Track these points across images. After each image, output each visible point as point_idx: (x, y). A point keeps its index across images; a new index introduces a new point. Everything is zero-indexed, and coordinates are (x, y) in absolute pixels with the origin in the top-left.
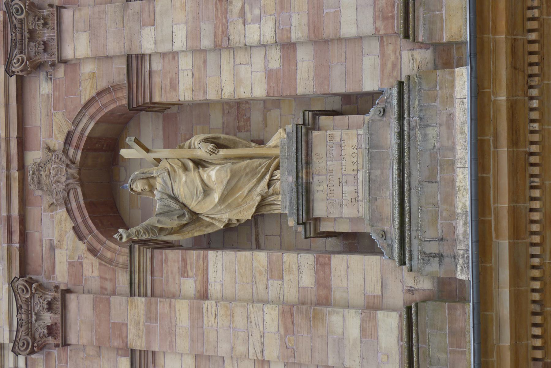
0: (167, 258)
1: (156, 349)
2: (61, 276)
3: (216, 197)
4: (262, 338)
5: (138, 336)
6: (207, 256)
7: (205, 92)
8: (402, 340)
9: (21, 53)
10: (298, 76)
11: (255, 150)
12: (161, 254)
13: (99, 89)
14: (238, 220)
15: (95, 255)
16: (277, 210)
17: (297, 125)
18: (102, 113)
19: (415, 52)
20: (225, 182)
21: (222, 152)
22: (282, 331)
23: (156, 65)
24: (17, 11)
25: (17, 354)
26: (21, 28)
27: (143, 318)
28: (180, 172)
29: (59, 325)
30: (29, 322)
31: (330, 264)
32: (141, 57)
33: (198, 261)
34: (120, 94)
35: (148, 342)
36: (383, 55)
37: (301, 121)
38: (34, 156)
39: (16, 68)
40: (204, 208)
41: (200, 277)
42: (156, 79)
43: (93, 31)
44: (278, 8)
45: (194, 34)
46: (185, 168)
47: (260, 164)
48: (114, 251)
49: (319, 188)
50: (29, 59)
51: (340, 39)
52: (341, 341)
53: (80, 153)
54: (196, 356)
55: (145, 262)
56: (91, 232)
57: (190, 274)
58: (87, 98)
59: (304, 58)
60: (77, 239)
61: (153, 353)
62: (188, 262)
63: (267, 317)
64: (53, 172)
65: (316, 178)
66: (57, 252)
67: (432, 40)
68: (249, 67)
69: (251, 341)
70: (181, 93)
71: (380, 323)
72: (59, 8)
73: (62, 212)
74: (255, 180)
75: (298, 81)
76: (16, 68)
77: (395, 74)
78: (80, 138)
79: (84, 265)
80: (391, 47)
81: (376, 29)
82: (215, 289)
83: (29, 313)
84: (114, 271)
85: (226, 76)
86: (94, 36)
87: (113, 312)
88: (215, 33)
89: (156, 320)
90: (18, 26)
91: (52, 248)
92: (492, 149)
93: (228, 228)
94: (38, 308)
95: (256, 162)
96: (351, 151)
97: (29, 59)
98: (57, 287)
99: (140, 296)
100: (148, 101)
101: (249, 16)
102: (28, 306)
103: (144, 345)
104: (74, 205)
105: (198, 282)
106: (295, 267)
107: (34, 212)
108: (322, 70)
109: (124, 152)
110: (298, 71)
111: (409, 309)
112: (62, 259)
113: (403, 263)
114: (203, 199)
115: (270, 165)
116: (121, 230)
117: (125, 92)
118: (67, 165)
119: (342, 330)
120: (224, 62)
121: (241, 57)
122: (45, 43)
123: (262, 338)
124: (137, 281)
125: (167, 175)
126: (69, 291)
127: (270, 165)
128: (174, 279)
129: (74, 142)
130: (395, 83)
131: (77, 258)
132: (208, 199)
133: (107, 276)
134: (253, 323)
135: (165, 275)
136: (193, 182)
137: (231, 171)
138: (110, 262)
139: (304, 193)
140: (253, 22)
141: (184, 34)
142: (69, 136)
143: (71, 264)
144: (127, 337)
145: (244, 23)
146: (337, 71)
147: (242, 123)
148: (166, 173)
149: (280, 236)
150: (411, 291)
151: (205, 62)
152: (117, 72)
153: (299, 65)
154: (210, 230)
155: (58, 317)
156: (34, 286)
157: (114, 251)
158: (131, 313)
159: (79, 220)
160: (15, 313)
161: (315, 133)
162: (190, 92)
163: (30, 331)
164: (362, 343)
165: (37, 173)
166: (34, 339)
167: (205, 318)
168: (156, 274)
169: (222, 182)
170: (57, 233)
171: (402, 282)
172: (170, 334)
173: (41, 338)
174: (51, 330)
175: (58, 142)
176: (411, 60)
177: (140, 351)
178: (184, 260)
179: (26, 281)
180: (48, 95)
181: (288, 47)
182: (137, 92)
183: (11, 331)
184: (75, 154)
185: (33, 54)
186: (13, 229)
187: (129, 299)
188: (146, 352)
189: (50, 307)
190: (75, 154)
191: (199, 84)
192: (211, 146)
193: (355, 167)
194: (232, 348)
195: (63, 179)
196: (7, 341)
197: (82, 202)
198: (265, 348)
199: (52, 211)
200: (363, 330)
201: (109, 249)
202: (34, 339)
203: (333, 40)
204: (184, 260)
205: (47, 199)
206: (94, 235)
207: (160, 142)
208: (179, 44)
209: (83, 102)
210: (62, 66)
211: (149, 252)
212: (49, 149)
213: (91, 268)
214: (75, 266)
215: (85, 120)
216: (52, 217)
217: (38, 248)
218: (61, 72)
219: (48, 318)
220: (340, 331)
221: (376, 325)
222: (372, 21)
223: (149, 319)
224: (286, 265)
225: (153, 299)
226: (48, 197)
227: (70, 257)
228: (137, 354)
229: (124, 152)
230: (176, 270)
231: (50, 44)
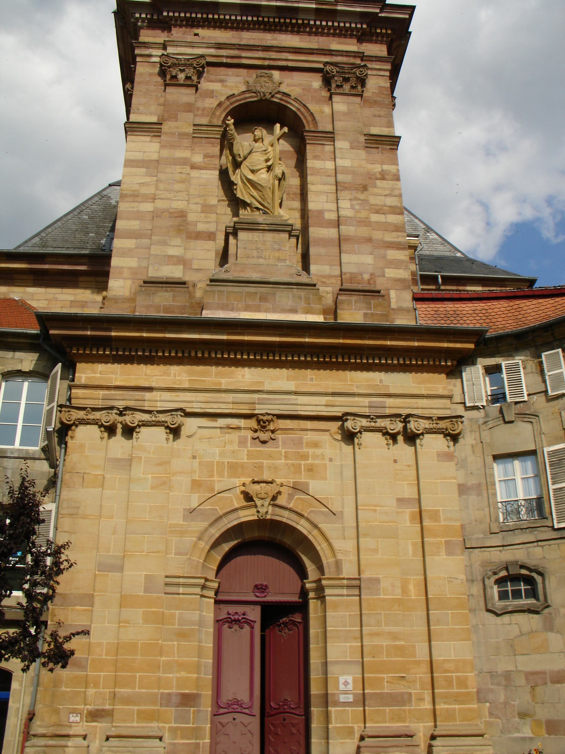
0: (216, 146)
2: (204, 85)
3: (251, 176)
4: (168, 199)
5: (170, 128)
6: (216, 170)
7: (312, 175)
8: (166, 278)
9: (337, 72)
11: (277, 202)
12: (217, 144)
13: (315, 115)
14: (236, 189)
15: (218, 105)
16: (242, 212)
17: (292, 226)
19: (331, 294)
20: (259, 182)
22: (172, 210)
23: (328, 148)
24: (361, 72)
25: (160, 57)
26: (351, 73)
28: (266, 157)
29: (177, 82)
30: (179, 65)
31: (210, 240)
32: (333, 140)
33: (213, 164)
34: (311, 126)
35: (166, 133)
36: (330, 276)
38: (276, 74)
39: (328, 68)
40: (244, 169)
41: (203, 165)
42: (319, 147)
44: (358, 219)
45: (346, 170)
46: (267, 160)
47: (269, 203)
48: (220, 116)
49: (255, 236)
50: (334, 76)
51: (340, 253)
52: (165, 243)
53: (278, 101)
54: (158, 161)
56: (231, 104)
57: (206, 160)
59: (332, 233)
60: (227, 96)
61: (160, 136)
63: (180, 202)
64: (267, 84)
66: (220, 84)
68: (325, 200)
69: (166, 192)
71: (176, 267)
72: (361, 96)
73: (244, 89)
74: (260, 199)
75: (317, 228)
76: (328, 68)
77: (319, 283)
78: (287, 102)
79: (212, 99)
80: (334, 281)
81: (345, 273)
82: (195, 173)
83: (185, 65)
84: (207, 116)
85: (321, 188)
86: (345, 114)
87: (185, 114)
88: (345, 183)
89: (180, 139)
90: (353, 71)
91: (222, 81)
92: (278, 332)
93: (232, 184)
95: (270, 201)
96: (277, 256)
97: (334, 76)
98: (199, 83)
99: (194, 130)
101: (354, 202)
102: (189, 65)
106: (209, 220)
109: (278, 126)
110: (322, 229)
111: (184, 283)
112: (216, 86)
113: (211, 281)
116: (232, 121)
117: (313, 129)
118: (271, 93)
119: (172, 244)
120: (329, 187)
121: (332, 197)
122: (342, 86)
123: (168, 199)
125: (263, 149)
126: (197, 90)
131: (216, 95)
132: (250, 172)
133: (205, 112)
134: (176, 194)
136: (260, 164)
137: (266, 186)
138: (213, 114)
139: (252, 227)
142: (288, 95)
143: (212, 91)
144: (169, 121)
145: (350, 200)
146: (322, 251)
147: (291, 196)
148: (264, 149)
149: (225, 214)
150: (194, 286)
151: (329, 176)
152: (325, 126)
153: (326, 229)
155: (182, 82)
156: (201, 69)
158: (184, 124)
159: (238, 98)
161: (287, 236)
162: (312, 166)
163: (174, 65)
164: (165, 256)
165: (267, 75)
166: (169, 67)
169: (259, 180)
170: (229, 86)
171: (200, 281)
172: (173, 146)
173: (170, 71)
175: (283, 88)
176: (328, 292)
177: (161, 129)
178: (213, 156)
179: (203, 64)
180: (311, 85)
181: (338, 223)
182: (313, 136)
183: (174, 54)
185: (336, 78)
186: (234, 59)
187: (192, 124)
188: (160, 132)
189: (188, 78)
191: (317, 172)
192: (280, 176)
193: (267, 257)
194: (162, 181)
195: (263, 91)
196: (168, 51)
199: (244, 83)
200: (171, 256)
201: (221, 114)
202: (169, 67)
204: (213, 156)
206: (229, 106)
207: (281, 149)
208: (339, 162)
209: (307, 105)
210: (328, 95)
211: (219, 137)
212: (280, 83)
213: (211, 103)
214: (211, 94)
215: (297, 105)
216: (240, 83)
218: (326, 94)
222: (350, 271)
224: (210, 215)
225: (191, 137)
226: (252, 81)
228: (160, 127)
229: (278, 126)
230: (208, 151)
231: (342, 89)
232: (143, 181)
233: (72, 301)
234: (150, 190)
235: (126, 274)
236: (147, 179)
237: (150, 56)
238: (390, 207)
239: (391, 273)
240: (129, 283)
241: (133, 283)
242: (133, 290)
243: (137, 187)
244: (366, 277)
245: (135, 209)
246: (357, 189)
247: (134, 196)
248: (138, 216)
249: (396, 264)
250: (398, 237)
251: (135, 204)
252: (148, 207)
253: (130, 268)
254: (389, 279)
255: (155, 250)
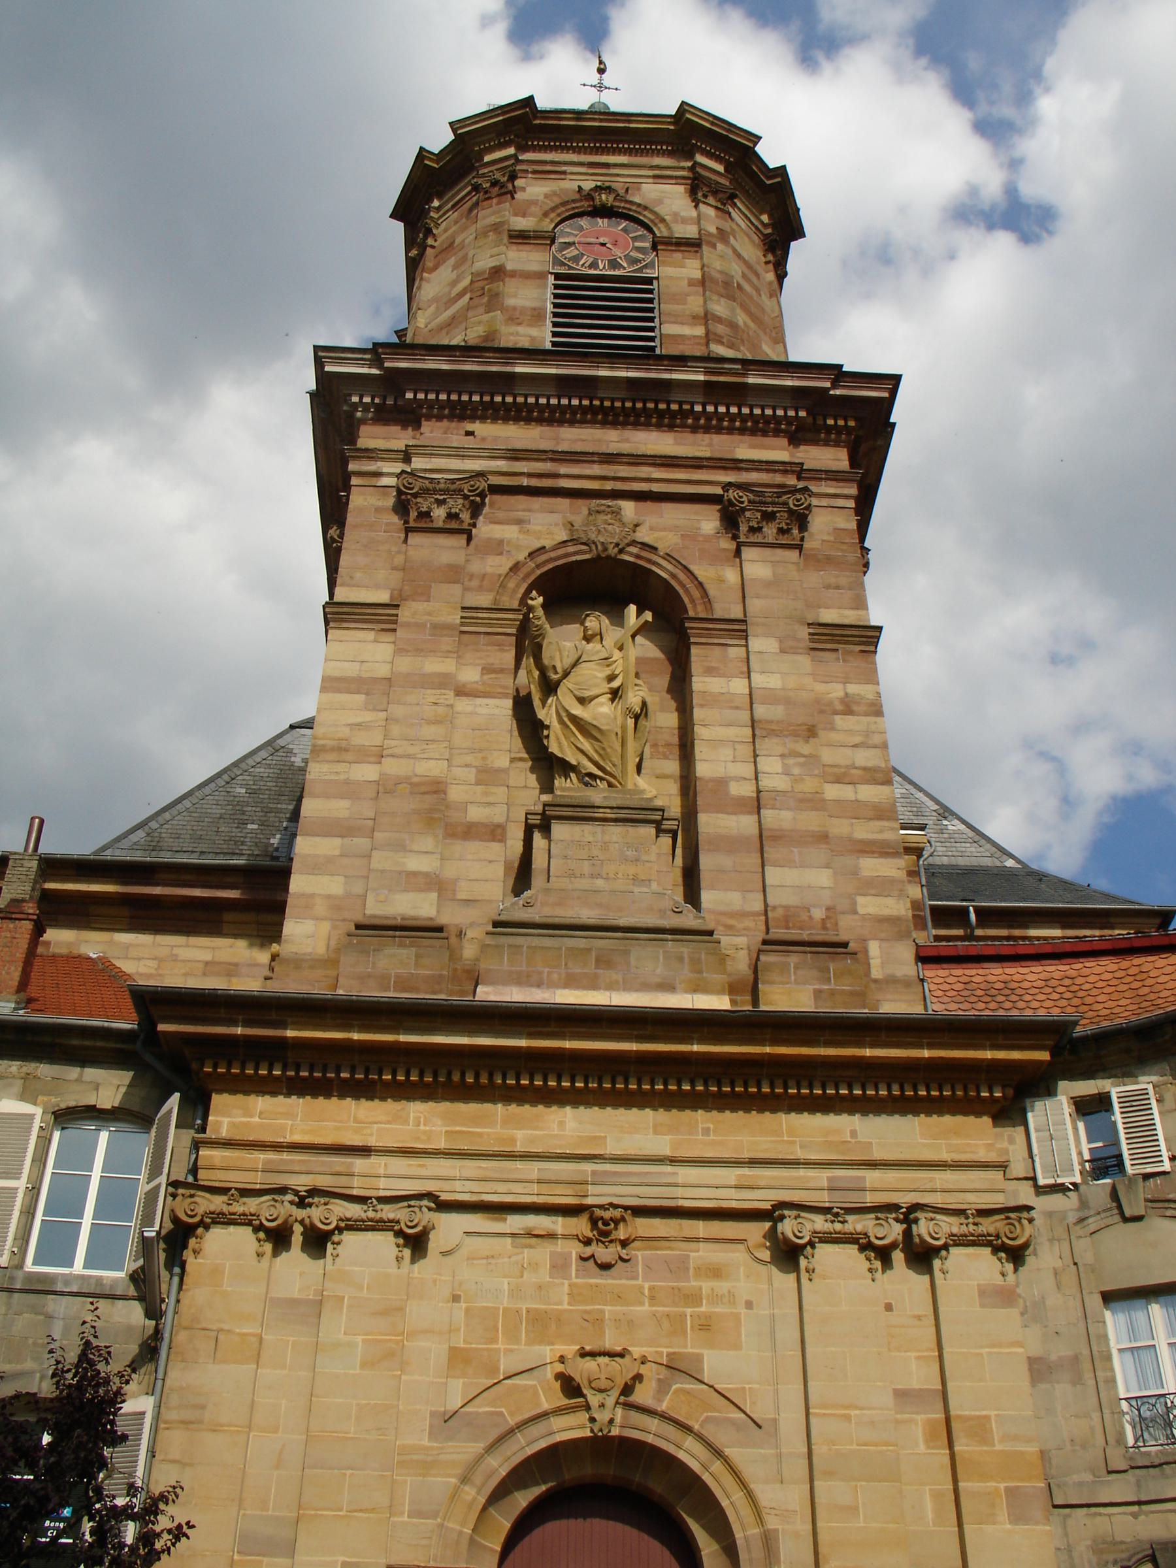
1: (398, 633)
2: (485, 529)
3: (578, 710)
4: (409, 756)
7: (702, 706)
8: (403, 919)
9: (749, 501)
10: (720, 815)
13: (707, 586)
14: (547, 737)
15: (511, 569)
16: (559, 782)
18: (678, 588)
20: (595, 723)
21: (631, 722)
22: (416, 780)
24: (798, 500)
25: (398, 476)
27: (436, 620)
28: (608, 672)
31: (493, 841)
34: (700, 608)
35: (407, 625)
36: (743, 915)
37: (666, 815)
38: (628, 508)
40: (565, 697)
41: (481, 688)
42: (717, 651)
43: (772, 584)
44: (800, 796)
45: (772, 697)
46: (611, 678)
47: (614, 765)
48: (514, 591)
50: (743, 510)
52: (401, 847)
54: (389, 679)
55: (501, 626)
56: (538, 566)
57: (486, 677)
58: (696, 572)
59: (745, 824)
61: (394, 630)
62: (499, 676)
63: (432, 763)
65: (599, 829)
66: (515, 528)
67: (336, 987)
68: (731, 758)
70: (701, 679)
71: (423, 895)
72: (800, 547)
73: (563, 536)
74: (596, 757)
76: (732, 494)
77: (721, 928)
78: (649, 561)
81: (774, 908)
82: (464, 705)
83: (446, 491)
84: (490, 590)
86: (767, 584)
87: (445, 586)
88: (772, 722)
91: (519, 522)
94: (451, 502)
97: (743, 510)
98: (474, 525)
100: (692, 640)
101: (791, 761)
103: (405, 620)
104: (571, 549)
105: (475, 686)
106: (491, 799)
107: (563, 503)
108: (731, 844)
110: (725, 816)
111: (440, 929)
112: (509, 532)
114: (575, 696)
115: (614, 777)
116: (541, 599)
117: (702, 615)
118: (617, 545)
121: (745, 751)
122: (760, 529)
123: (409, 756)
124: (480, 615)
125: (603, 656)
126: (469, 539)
127: (614, 777)
128: (480, 658)
129: (644, 554)
130: (710, 927)
133: (485, 582)
135: (485, 648)
136: (596, 685)
137: (608, 730)
138: (502, 586)
139: (580, 813)
140: (784, 765)
141: (771, 686)
143: (501, 542)
145: (782, 756)
146: (726, 861)
147: (661, 749)
149: (526, 787)
150: (460, 934)
151: (737, 708)
153: (733, 817)
154: (537, 702)
155: (440, 524)
156: (478, 499)
157: (514, 591)
158: (443, 606)
159: (553, 555)
160: (446, 476)
163: (425, 492)
164: (400, 873)
166: (415, 495)
167: (433, 691)
168: (487, 637)
170: (536, 531)
171: (472, 924)
172: (420, 651)
174: (425, 515)
175: (643, 535)
176: (738, 947)
177: (397, 615)
179: (483, 490)
181: (757, 805)
183: (426, 470)
184: (631, 554)
185: (748, 514)
187: (459, 606)
188: (396, 622)
189: (452, 516)
190: (631, 554)
191: (714, 700)
193: (611, 875)
196: (413, 465)
197: (574, 558)
198: (396, 759)
199: (564, 525)
200: (414, 874)
201: (518, 586)
202: (415, 495)
203: (762, 857)
205: (578, 520)
208: (758, 680)
209: (692, 567)
210: (733, 546)
211: (514, 631)
212: (636, 526)
213: (498, 565)
214: (498, 547)
215: (670, 567)
216: (557, 525)
217: (521, 507)
218: (728, 545)
219: (439, 513)
220: (416, 848)
221: (421, 890)
222: (784, 903)
223: (435, 627)
224: (494, 789)
227: (509, 542)
228: (394, 612)
229: (632, 608)
230: (491, 660)
232: (358, 720)
233: (207, 963)
234: (373, 738)
235: (320, 908)
236: (367, 717)
237: (378, 474)
238: (865, 769)
239: (869, 905)
240: (326, 927)
241: (334, 927)
242: (333, 943)
243: (345, 732)
244: (818, 914)
245: (342, 777)
246: (795, 734)
247: (340, 749)
248: (348, 790)
249: (880, 887)
250: (881, 831)
251: (341, 767)
252: (367, 772)
253: (329, 897)
254: (864, 917)
255: (380, 860)
